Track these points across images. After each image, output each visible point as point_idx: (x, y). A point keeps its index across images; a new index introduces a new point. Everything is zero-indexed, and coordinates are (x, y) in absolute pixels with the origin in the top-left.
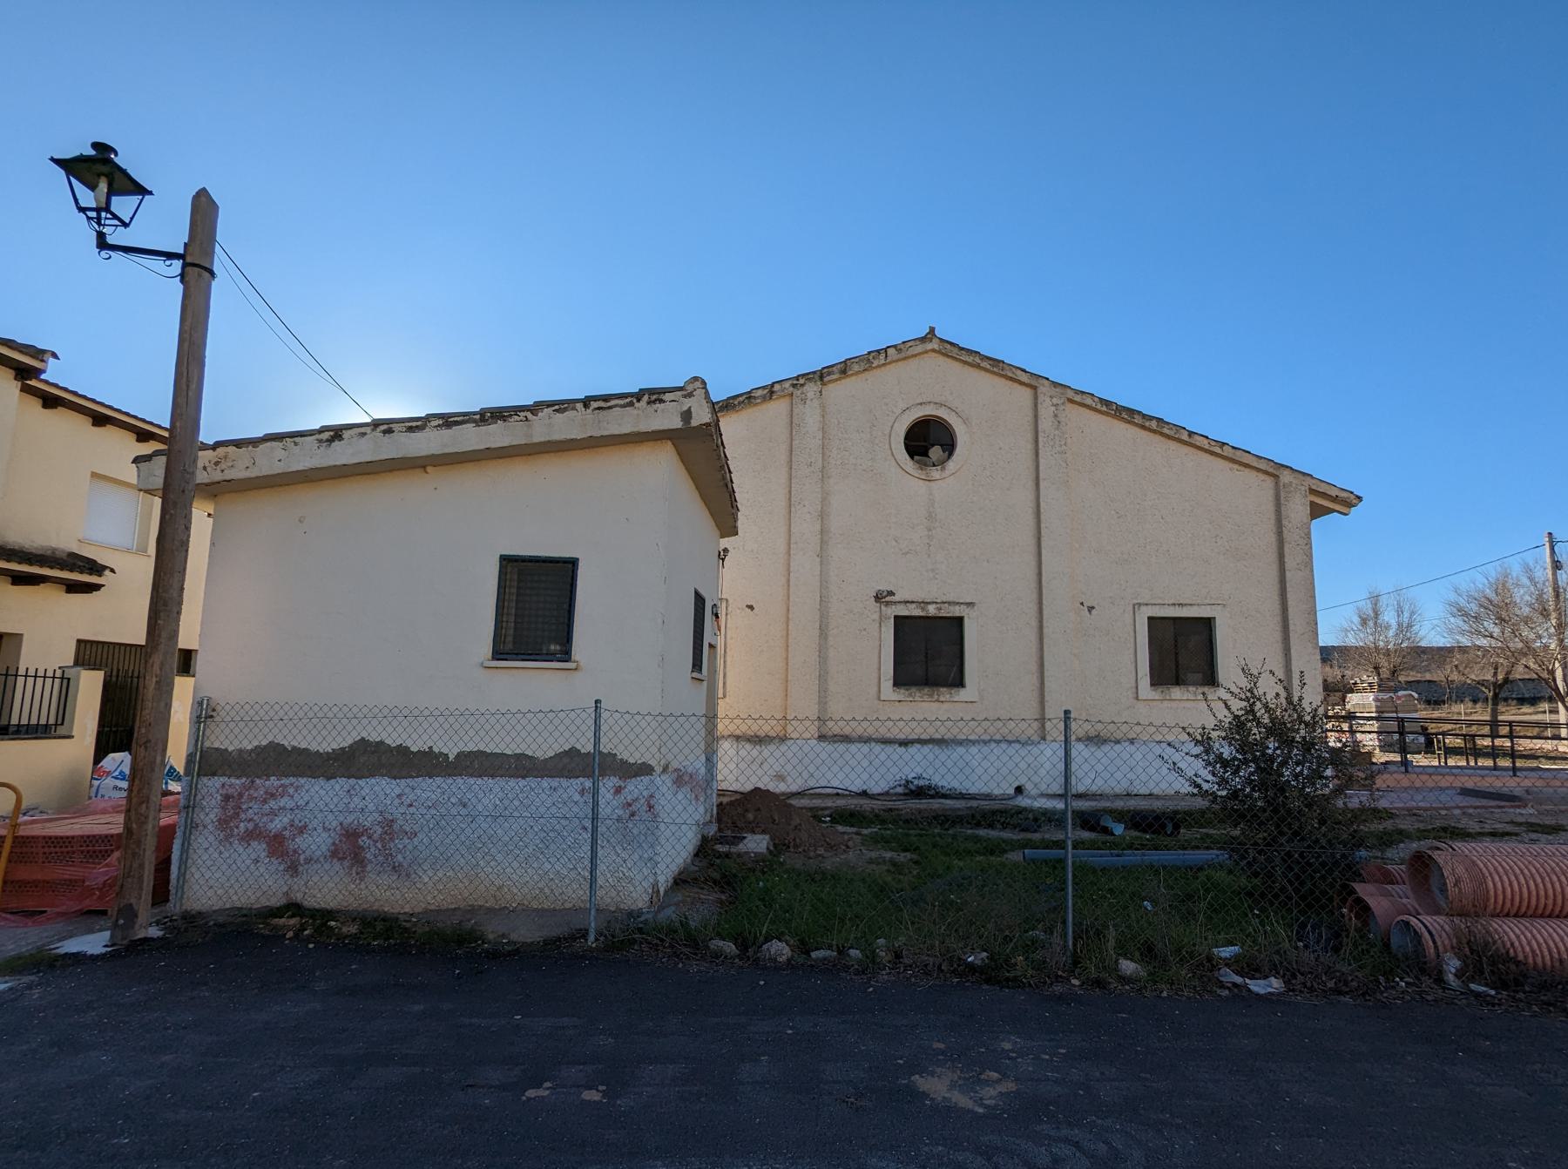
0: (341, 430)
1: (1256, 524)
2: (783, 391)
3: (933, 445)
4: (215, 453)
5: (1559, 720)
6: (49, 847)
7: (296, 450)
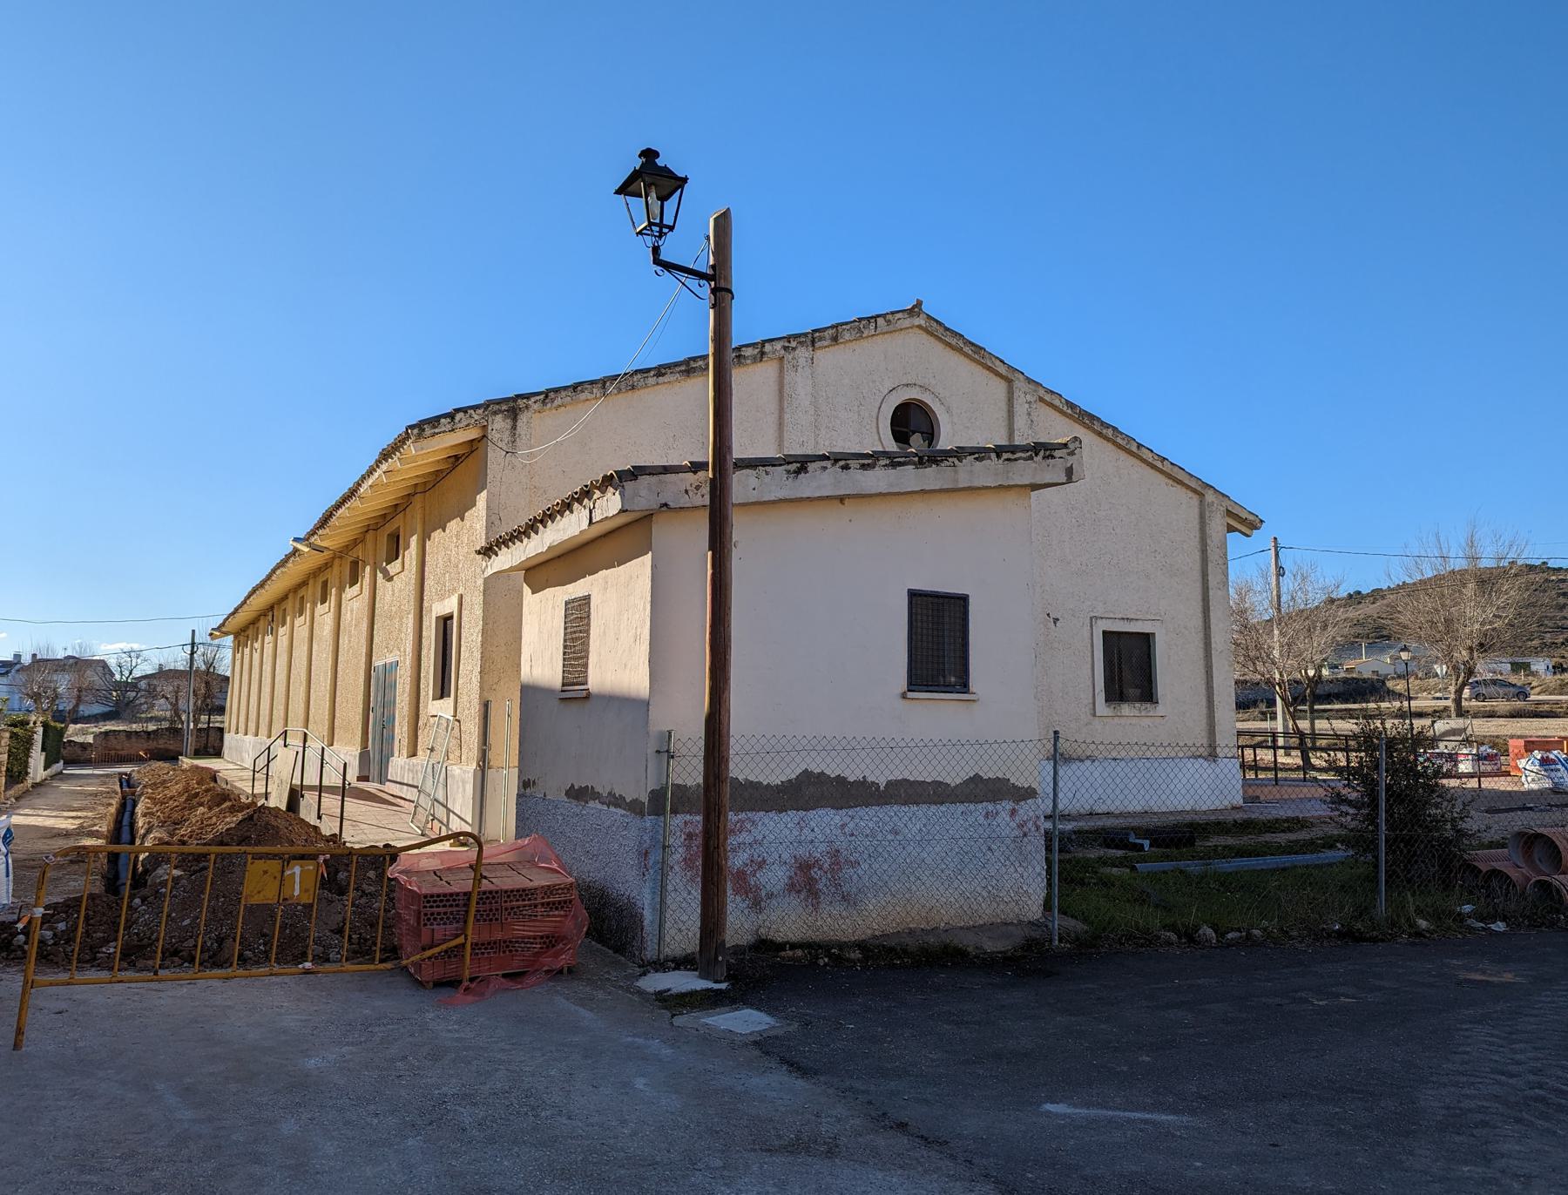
0: (806, 462)
1: (1184, 541)
2: (774, 353)
3: (914, 433)
4: (696, 477)
5: (1277, 729)
6: (511, 901)
7: (767, 479)
